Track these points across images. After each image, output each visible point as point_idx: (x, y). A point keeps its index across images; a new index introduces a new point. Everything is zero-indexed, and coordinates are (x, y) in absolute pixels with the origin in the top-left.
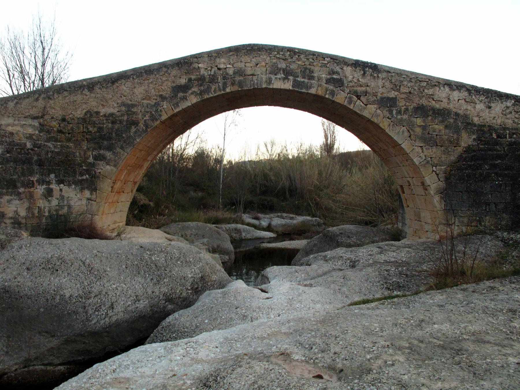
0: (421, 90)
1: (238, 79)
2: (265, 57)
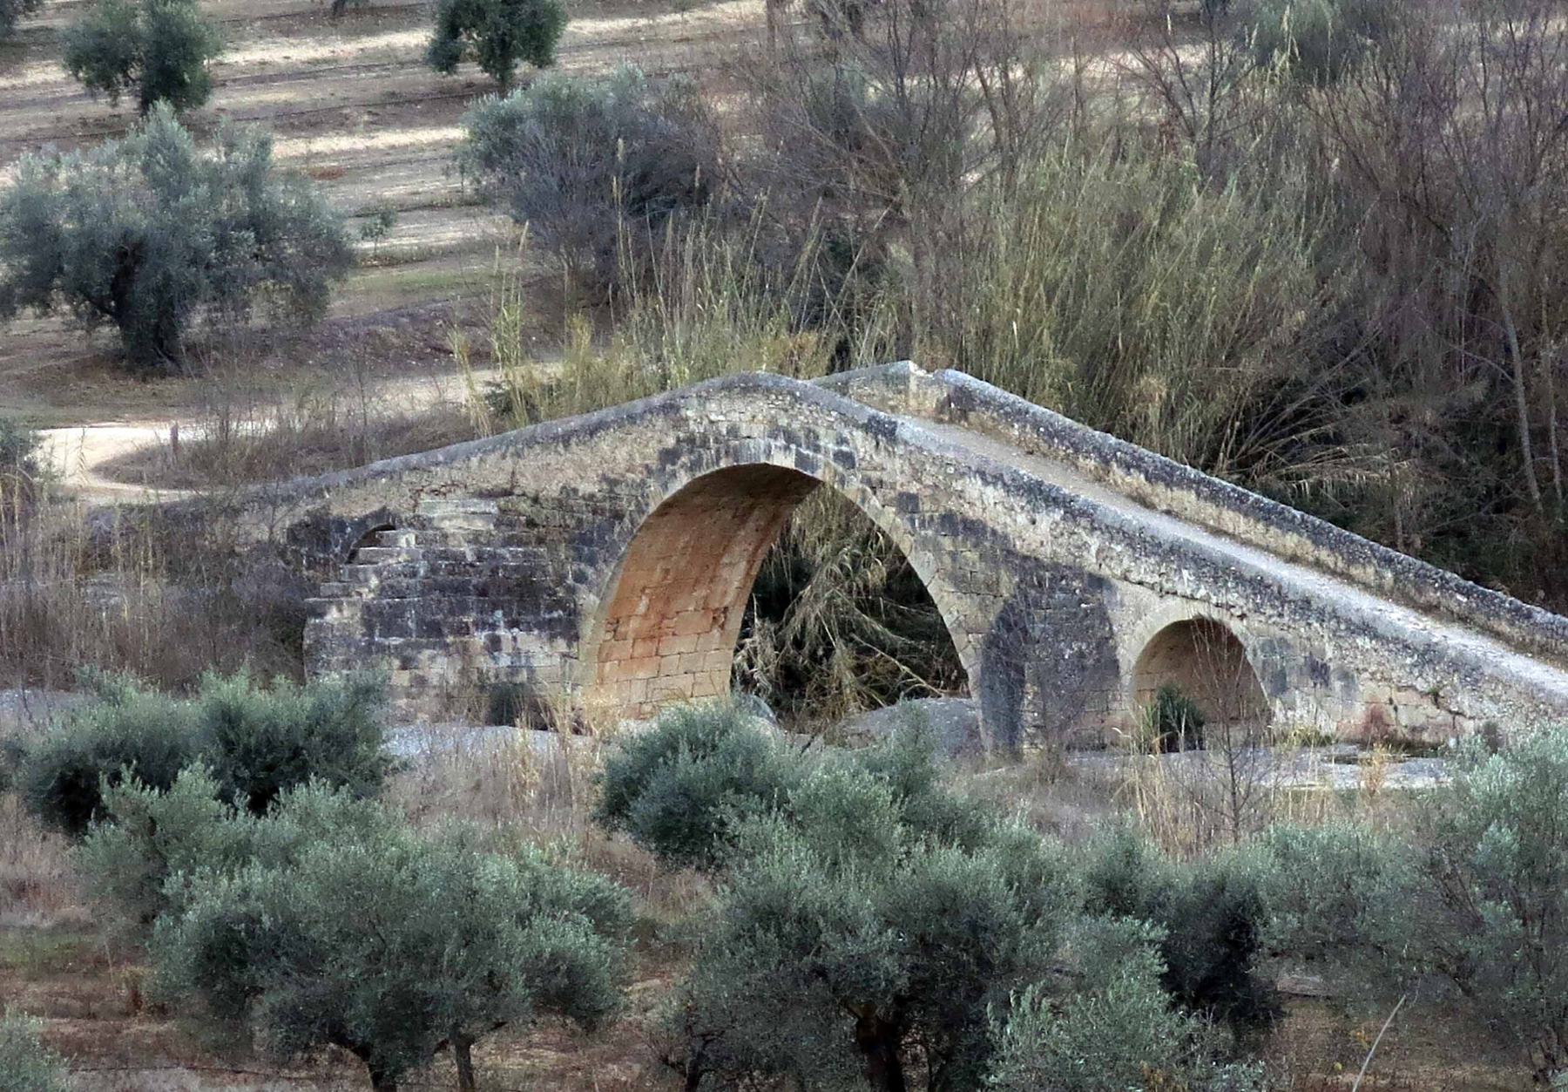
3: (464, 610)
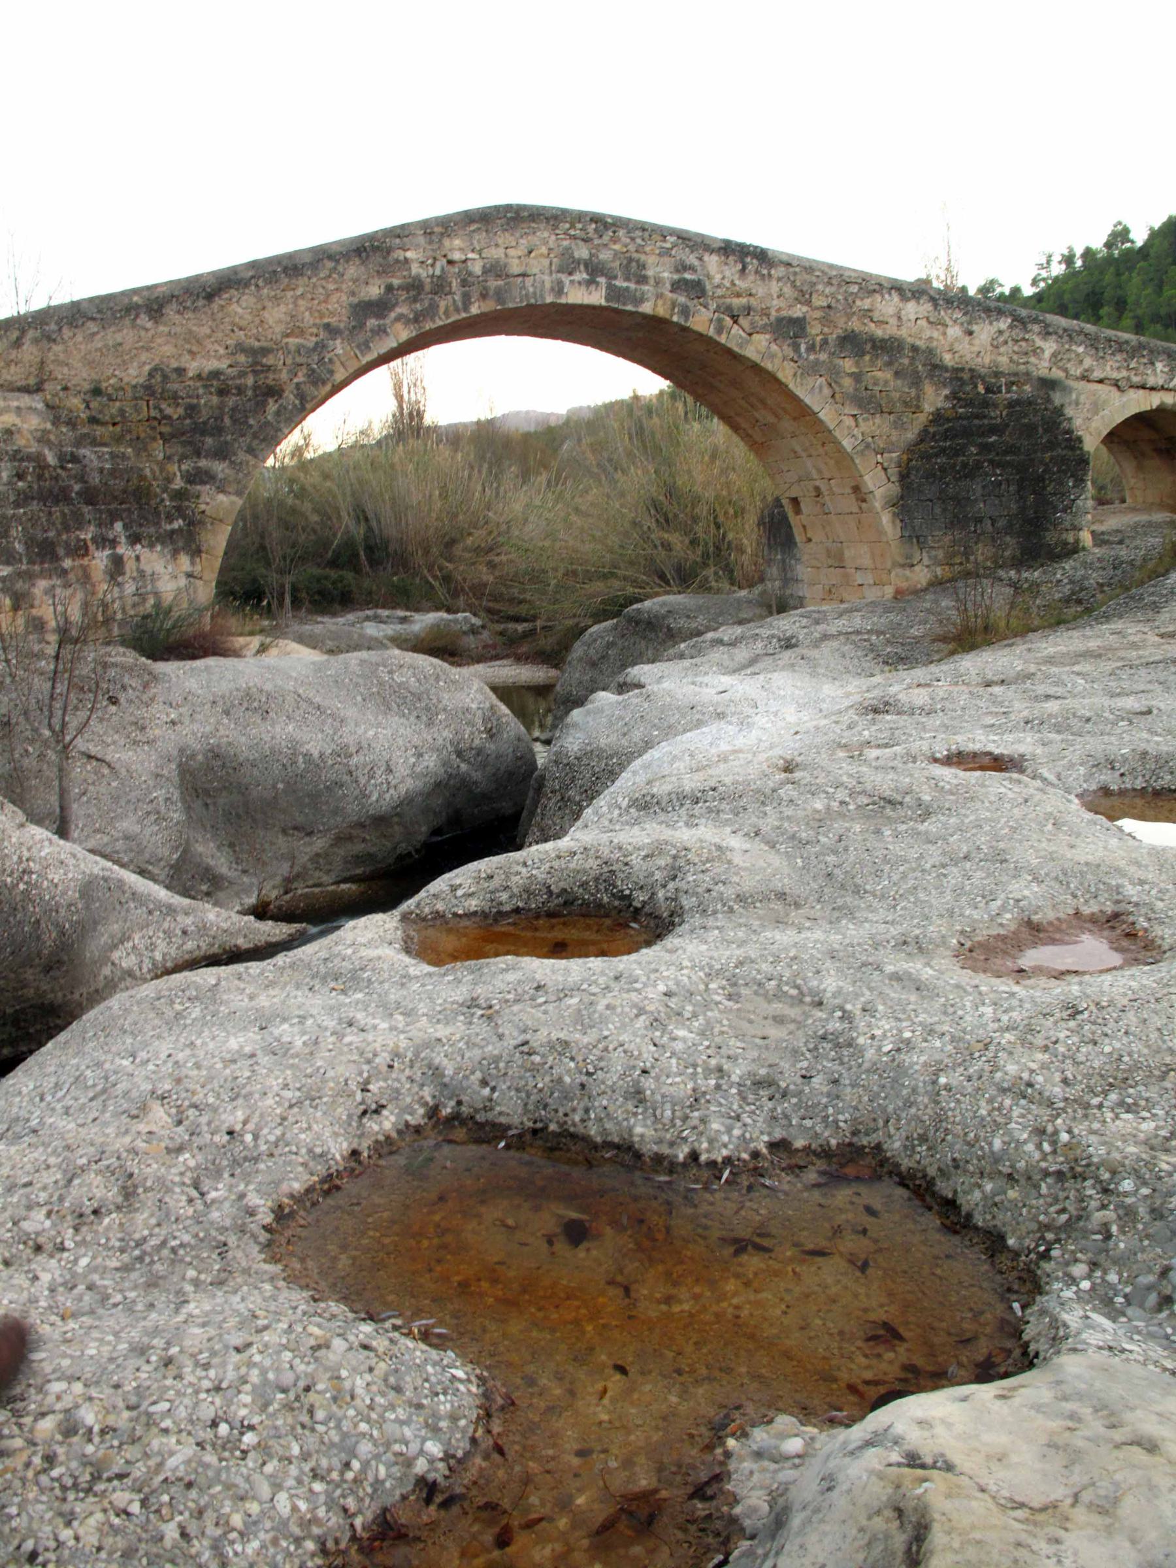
0: (849, 303)
1: (493, 284)
2: (546, 234)
3: (80, 524)
